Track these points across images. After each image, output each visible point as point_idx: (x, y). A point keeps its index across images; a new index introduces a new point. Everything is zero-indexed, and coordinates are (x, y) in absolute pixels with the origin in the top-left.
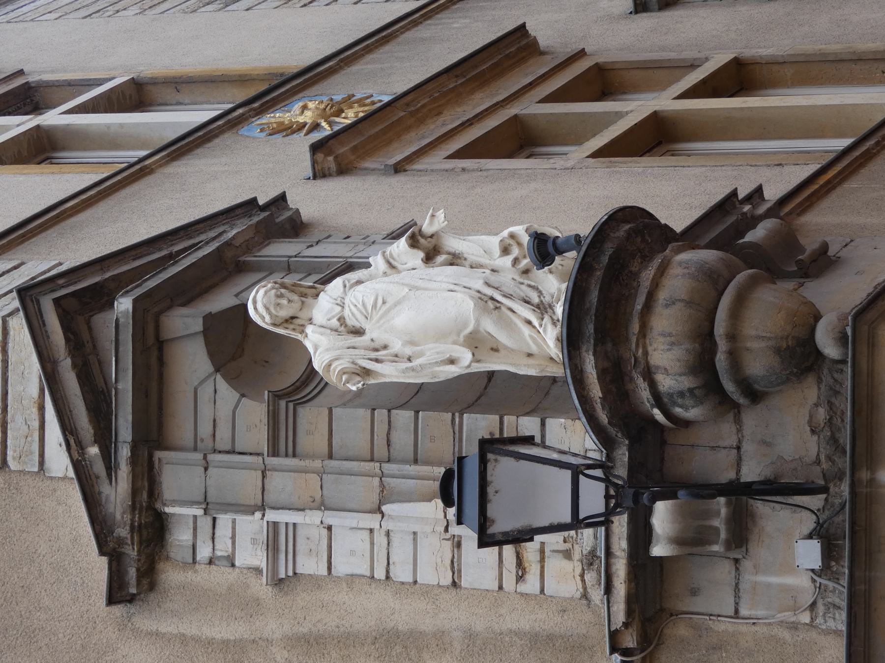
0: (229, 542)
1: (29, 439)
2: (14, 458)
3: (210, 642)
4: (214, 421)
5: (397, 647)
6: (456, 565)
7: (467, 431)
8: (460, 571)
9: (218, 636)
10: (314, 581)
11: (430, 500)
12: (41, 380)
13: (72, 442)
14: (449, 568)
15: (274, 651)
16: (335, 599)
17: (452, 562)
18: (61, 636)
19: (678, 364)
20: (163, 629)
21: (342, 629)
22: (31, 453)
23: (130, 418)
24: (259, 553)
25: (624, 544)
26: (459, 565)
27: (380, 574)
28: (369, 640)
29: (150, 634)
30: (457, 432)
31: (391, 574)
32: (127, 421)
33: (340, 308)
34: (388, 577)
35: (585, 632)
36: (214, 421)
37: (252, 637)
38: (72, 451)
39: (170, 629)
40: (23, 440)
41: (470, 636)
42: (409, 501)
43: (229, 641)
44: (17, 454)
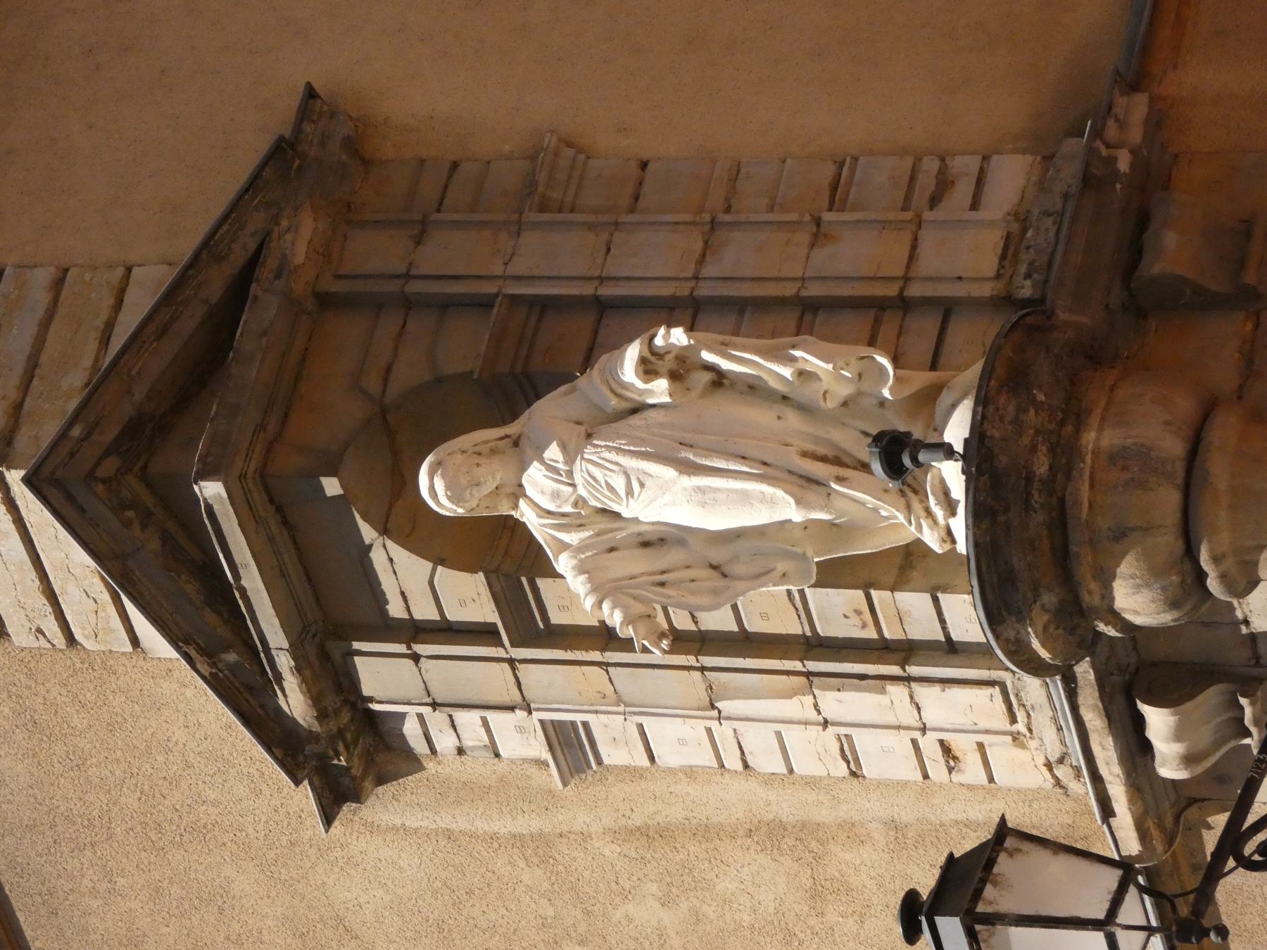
0: (482, 731)
1: (101, 614)
2: (86, 637)
3: (494, 837)
4: (403, 594)
5: (787, 840)
6: (848, 753)
7: (818, 615)
8: (857, 760)
9: (503, 831)
10: (631, 773)
11: (790, 697)
12: (103, 579)
13: (193, 653)
14: (840, 758)
15: (597, 845)
16: (672, 789)
17: (842, 750)
18: (251, 831)
19: (1153, 606)
20: (412, 822)
21: (694, 822)
22: (113, 631)
23: (276, 621)
24: (533, 741)
25: (1117, 769)
26: (854, 751)
27: (733, 762)
28: (741, 833)
29: (395, 829)
30: (850, 758)
31: (750, 763)
32: (272, 625)
33: (570, 489)
34: (746, 766)
35: (1070, 822)
36: (403, 594)
37: (558, 831)
38: (198, 666)
39: (425, 823)
40: (92, 617)
41: (895, 827)
42: (758, 698)
43: (521, 836)
44: (89, 631)
